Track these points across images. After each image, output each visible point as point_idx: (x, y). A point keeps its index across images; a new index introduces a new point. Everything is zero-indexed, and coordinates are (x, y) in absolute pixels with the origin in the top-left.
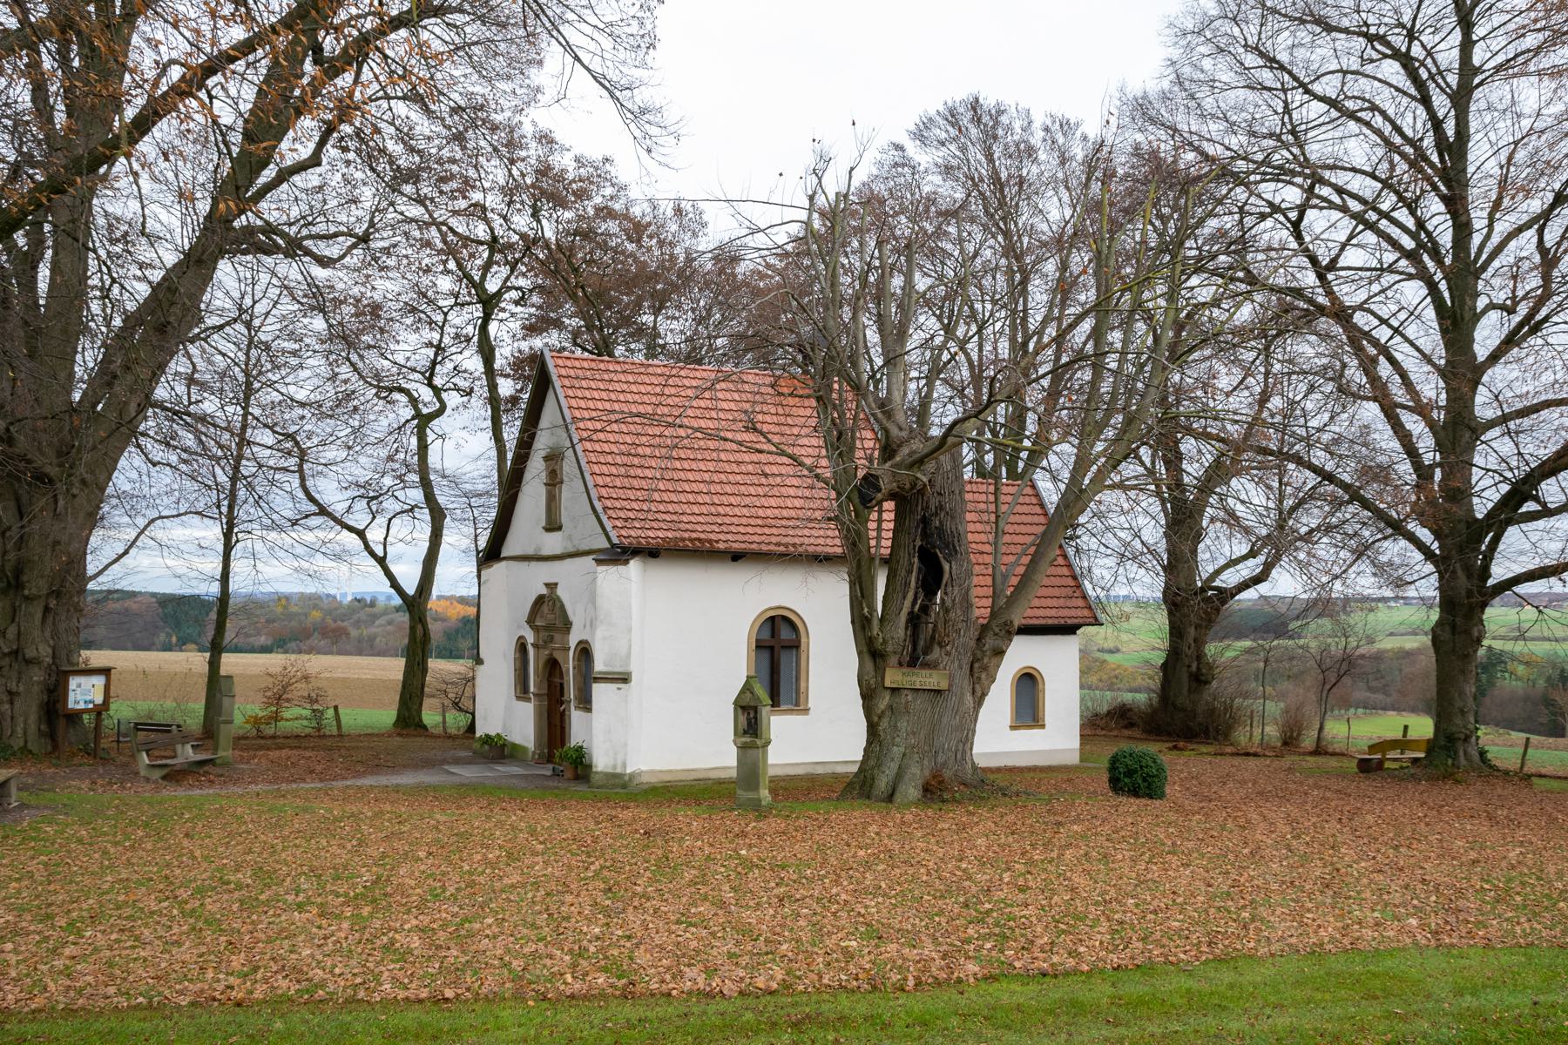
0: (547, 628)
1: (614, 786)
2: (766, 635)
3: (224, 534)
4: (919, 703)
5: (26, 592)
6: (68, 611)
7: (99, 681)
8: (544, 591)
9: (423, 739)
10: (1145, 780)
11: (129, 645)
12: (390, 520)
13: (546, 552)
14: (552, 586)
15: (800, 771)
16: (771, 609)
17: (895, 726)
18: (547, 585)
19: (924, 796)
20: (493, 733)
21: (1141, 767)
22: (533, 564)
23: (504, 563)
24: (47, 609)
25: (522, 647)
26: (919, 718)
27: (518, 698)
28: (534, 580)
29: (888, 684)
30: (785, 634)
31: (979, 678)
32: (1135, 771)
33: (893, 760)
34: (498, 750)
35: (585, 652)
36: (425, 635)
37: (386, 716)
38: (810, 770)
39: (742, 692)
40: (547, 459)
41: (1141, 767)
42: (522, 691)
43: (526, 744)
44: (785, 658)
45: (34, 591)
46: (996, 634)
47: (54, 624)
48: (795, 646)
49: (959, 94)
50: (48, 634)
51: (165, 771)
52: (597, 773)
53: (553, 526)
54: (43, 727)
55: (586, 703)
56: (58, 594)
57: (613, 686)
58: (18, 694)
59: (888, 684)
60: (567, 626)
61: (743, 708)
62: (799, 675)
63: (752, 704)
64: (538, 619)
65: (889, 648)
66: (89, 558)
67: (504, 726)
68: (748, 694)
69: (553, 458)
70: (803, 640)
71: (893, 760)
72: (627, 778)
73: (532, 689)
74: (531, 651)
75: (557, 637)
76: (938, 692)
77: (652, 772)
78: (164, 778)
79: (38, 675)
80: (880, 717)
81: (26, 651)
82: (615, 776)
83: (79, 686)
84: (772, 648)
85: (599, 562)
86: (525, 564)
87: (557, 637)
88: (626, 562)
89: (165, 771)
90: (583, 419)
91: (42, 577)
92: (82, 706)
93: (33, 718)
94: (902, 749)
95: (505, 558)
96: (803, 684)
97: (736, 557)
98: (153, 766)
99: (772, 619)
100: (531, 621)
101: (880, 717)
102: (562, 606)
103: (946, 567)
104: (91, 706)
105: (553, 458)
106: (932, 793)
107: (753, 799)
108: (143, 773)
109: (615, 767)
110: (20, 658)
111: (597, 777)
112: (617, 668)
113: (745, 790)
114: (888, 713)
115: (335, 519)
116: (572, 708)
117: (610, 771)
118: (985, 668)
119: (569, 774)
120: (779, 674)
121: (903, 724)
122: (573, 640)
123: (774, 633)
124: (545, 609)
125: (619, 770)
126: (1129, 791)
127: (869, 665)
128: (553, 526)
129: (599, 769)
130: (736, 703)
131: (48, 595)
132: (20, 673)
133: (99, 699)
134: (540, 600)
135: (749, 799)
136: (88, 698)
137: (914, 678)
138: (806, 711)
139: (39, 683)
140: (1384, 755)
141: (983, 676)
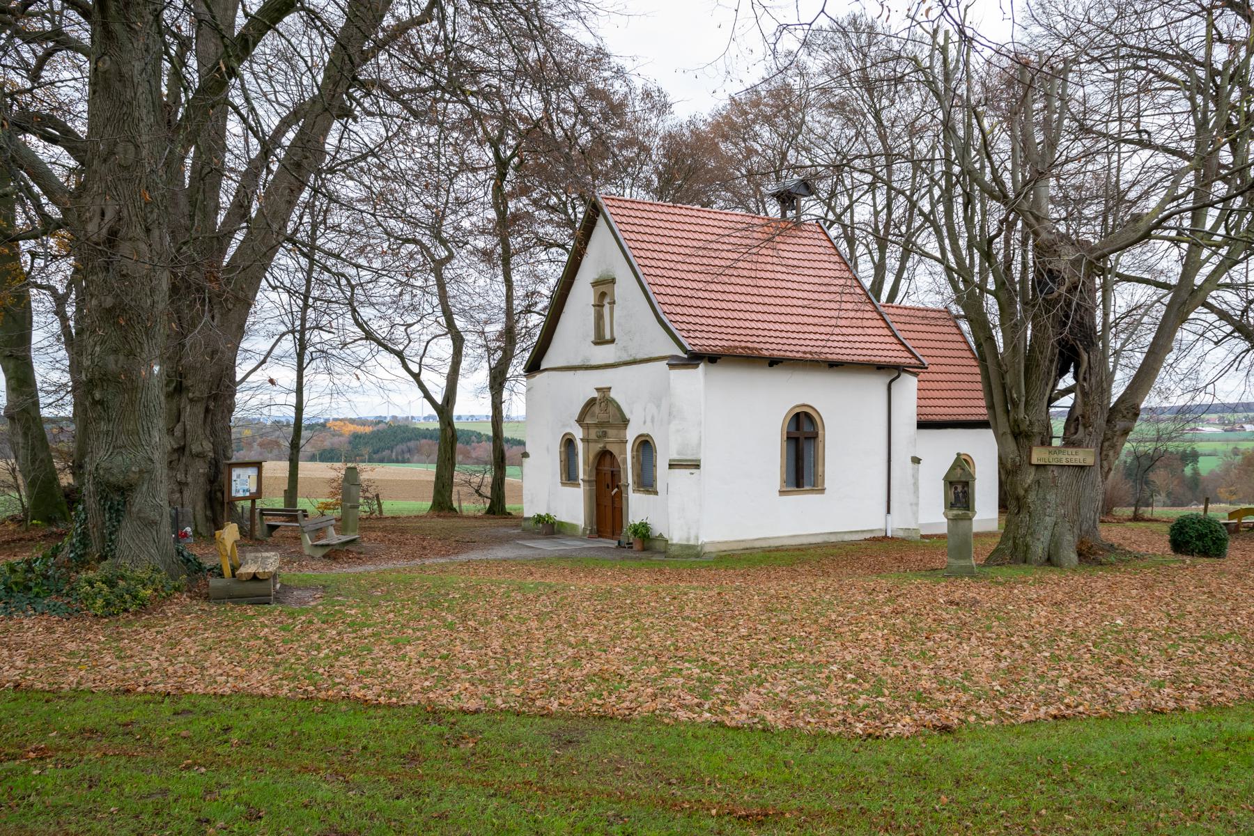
0: (600, 425)
1: (689, 556)
2: (793, 429)
3: (298, 355)
4: (1065, 478)
5: (190, 395)
6: (223, 412)
7: (252, 472)
8: (595, 394)
9: (456, 520)
10: (1214, 543)
11: (611, 409)
12: (428, 343)
13: (593, 363)
14: (604, 391)
15: (819, 540)
16: (798, 406)
17: (1045, 499)
18: (598, 390)
19: (1080, 560)
20: (543, 514)
21: (1211, 532)
22: (580, 373)
23: (546, 373)
24: (207, 410)
25: (569, 443)
26: (1067, 491)
27: (563, 484)
28: (585, 387)
29: (1034, 461)
30: (806, 428)
31: (1107, 455)
32: (1206, 535)
33: (1046, 528)
34: (549, 527)
35: (645, 444)
36: (453, 435)
37: (424, 504)
38: (826, 539)
39: (953, 468)
40: (595, 284)
41: (1211, 532)
42: (569, 476)
43: (574, 522)
44: (807, 448)
45: (197, 394)
46: (1124, 417)
47: (212, 423)
48: (814, 437)
49: (841, 9)
50: (208, 432)
51: (327, 550)
52: (672, 545)
53: (600, 340)
54: (209, 513)
55: (647, 484)
56: (215, 398)
57: (687, 471)
58: (186, 484)
59: (1034, 461)
60: (625, 422)
61: (951, 483)
62: (817, 461)
63: (963, 479)
64: (587, 418)
65: (1036, 430)
66: (237, 369)
67: (549, 508)
68: (959, 471)
69: (604, 286)
70: (820, 432)
71: (1046, 528)
72: (699, 549)
73: (581, 476)
74: (580, 446)
75: (611, 432)
76: (1082, 467)
77: (713, 543)
78: (324, 556)
79: (202, 468)
80: (1026, 491)
81: (193, 447)
82: (689, 547)
83: (239, 476)
84: (797, 440)
85: (672, 366)
86: (571, 373)
87: (611, 432)
88: (697, 366)
89: (327, 550)
90: (763, 226)
91: (204, 382)
92: (241, 494)
93: (200, 506)
94: (1054, 519)
95: (546, 370)
96: (820, 469)
97: (774, 362)
98: (316, 546)
99: (797, 415)
100: (580, 421)
101: (1026, 491)
102: (619, 408)
103: (1085, 357)
104: (248, 494)
105: (604, 286)
106: (1085, 557)
107: (966, 567)
108: (307, 552)
109: (688, 539)
110: (187, 452)
111: (673, 548)
112: (689, 456)
113: (957, 558)
114: (1035, 487)
115: (380, 343)
116: (630, 489)
117: (685, 543)
118: (1113, 447)
119: (637, 546)
120: (803, 460)
121: (1051, 497)
122: (631, 435)
123: (798, 428)
124: (596, 409)
125: (692, 542)
126: (1200, 552)
127: (1011, 444)
128: (600, 340)
129: (674, 542)
130: (946, 479)
131: (209, 397)
132: (187, 466)
133: (254, 489)
134: (591, 403)
135: (961, 567)
136: (246, 487)
137: (1061, 456)
138: (822, 491)
139: (204, 474)
140: (1240, 520)
141: (1111, 453)
